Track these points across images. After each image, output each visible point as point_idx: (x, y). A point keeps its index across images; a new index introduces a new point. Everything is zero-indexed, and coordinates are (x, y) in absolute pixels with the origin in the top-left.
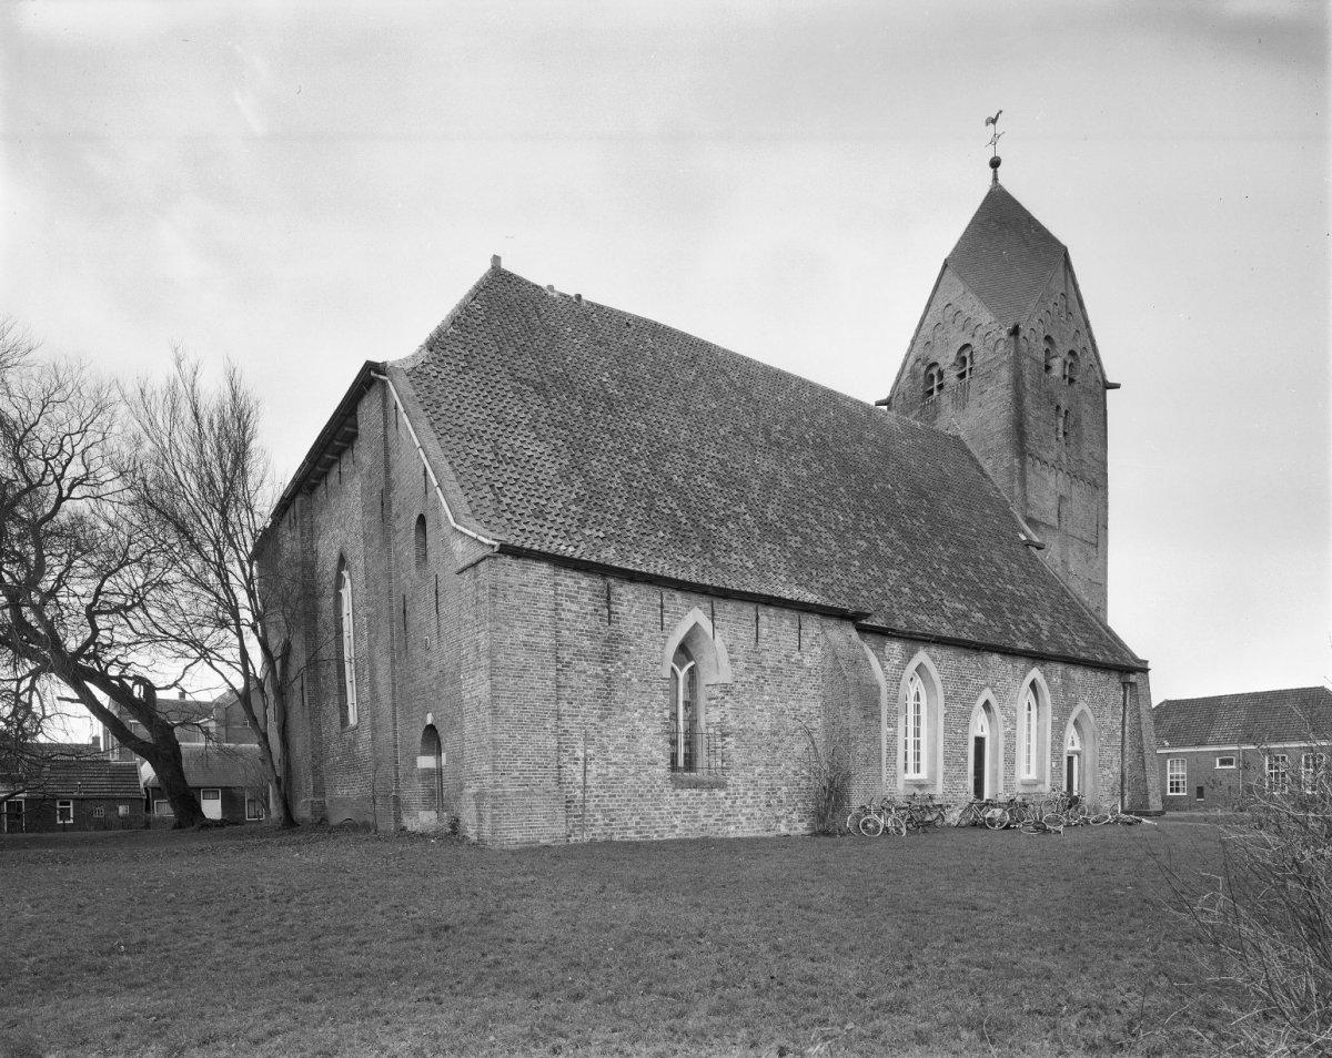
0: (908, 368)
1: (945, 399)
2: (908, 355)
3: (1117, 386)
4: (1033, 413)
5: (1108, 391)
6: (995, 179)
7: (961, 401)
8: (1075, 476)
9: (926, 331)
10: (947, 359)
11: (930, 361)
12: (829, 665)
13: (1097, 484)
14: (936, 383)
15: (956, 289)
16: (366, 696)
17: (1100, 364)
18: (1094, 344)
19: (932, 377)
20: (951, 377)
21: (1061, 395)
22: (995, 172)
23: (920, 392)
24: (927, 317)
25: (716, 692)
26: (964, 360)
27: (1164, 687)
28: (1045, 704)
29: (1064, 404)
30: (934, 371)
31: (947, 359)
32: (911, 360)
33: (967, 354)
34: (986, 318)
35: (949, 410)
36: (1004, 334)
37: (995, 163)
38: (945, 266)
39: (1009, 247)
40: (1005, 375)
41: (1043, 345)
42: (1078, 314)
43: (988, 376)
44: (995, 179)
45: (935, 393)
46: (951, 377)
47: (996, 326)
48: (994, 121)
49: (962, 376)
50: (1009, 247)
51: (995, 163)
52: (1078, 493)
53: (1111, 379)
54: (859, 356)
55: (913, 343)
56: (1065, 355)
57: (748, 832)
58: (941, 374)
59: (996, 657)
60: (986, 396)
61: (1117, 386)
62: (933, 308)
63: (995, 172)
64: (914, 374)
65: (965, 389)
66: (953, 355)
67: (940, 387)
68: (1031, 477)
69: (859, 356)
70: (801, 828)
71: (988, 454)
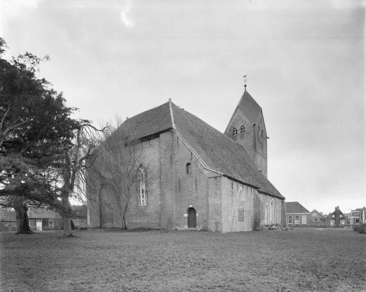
0: (229, 128)
1: (238, 137)
2: (229, 125)
3: (269, 138)
4: (257, 143)
5: (267, 139)
6: (245, 89)
7: (242, 137)
8: (263, 156)
9: (233, 120)
10: (238, 128)
11: (234, 127)
12: (255, 198)
13: (266, 158)
14: (235, 132)
15: (240, 113)
16: (146, 202)
17: (266, 133)
18: (265, 129)
19: (234, 131)
20: (239, 132)
21: (260, 139)
22: (245, 88)
23: (232, 134)
24: (234, 118)
25: (242, 203)
26: (242, 129)
27: (286, 201)
28: (273, 205)
29: (261, 141)
30: (235, 130)
31: (238, 128)
32: (229, 126)
33: (243, 127)
34: (248, 121)
35: (239, 139)
36: (252, 125)
37: (245, 86)
38: (238, 107)
39: (248, 104)
40: (252, 134)
41: (258, 128)
42: (263, 122)
43: (248, 133)
44: (245, 89)
45: (235, 135)
46: (239, 132)
47: (250, 123)
48: (245, 77)
49: (242, 132)
50: (248, 104)
51: (245, 86)
52: (263, 159)
53: (268, 136)
54: (220, 123)
55: (230, 122)
56: (261, 131)
57: (246, 231)
58: (237, 131)
59: (268, 196)
60: (248, 138)
61: (269, 138)
62: (235, 116)
63: (245, 88)
64: (230, 130)
65: (243, 135)
66: (240, 128)
67: (236, 133)
68: (257, 156)
69: (220, 123)
70: (251, 230)
71: (249, 150)
